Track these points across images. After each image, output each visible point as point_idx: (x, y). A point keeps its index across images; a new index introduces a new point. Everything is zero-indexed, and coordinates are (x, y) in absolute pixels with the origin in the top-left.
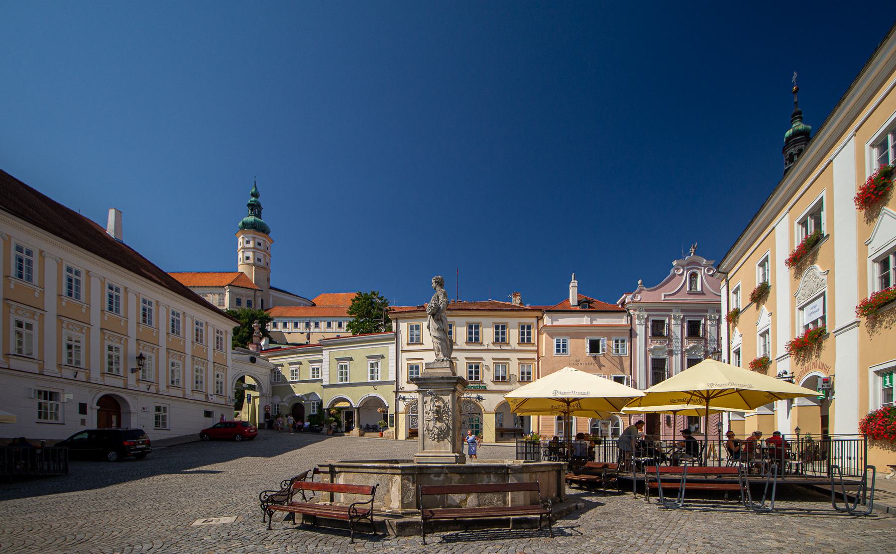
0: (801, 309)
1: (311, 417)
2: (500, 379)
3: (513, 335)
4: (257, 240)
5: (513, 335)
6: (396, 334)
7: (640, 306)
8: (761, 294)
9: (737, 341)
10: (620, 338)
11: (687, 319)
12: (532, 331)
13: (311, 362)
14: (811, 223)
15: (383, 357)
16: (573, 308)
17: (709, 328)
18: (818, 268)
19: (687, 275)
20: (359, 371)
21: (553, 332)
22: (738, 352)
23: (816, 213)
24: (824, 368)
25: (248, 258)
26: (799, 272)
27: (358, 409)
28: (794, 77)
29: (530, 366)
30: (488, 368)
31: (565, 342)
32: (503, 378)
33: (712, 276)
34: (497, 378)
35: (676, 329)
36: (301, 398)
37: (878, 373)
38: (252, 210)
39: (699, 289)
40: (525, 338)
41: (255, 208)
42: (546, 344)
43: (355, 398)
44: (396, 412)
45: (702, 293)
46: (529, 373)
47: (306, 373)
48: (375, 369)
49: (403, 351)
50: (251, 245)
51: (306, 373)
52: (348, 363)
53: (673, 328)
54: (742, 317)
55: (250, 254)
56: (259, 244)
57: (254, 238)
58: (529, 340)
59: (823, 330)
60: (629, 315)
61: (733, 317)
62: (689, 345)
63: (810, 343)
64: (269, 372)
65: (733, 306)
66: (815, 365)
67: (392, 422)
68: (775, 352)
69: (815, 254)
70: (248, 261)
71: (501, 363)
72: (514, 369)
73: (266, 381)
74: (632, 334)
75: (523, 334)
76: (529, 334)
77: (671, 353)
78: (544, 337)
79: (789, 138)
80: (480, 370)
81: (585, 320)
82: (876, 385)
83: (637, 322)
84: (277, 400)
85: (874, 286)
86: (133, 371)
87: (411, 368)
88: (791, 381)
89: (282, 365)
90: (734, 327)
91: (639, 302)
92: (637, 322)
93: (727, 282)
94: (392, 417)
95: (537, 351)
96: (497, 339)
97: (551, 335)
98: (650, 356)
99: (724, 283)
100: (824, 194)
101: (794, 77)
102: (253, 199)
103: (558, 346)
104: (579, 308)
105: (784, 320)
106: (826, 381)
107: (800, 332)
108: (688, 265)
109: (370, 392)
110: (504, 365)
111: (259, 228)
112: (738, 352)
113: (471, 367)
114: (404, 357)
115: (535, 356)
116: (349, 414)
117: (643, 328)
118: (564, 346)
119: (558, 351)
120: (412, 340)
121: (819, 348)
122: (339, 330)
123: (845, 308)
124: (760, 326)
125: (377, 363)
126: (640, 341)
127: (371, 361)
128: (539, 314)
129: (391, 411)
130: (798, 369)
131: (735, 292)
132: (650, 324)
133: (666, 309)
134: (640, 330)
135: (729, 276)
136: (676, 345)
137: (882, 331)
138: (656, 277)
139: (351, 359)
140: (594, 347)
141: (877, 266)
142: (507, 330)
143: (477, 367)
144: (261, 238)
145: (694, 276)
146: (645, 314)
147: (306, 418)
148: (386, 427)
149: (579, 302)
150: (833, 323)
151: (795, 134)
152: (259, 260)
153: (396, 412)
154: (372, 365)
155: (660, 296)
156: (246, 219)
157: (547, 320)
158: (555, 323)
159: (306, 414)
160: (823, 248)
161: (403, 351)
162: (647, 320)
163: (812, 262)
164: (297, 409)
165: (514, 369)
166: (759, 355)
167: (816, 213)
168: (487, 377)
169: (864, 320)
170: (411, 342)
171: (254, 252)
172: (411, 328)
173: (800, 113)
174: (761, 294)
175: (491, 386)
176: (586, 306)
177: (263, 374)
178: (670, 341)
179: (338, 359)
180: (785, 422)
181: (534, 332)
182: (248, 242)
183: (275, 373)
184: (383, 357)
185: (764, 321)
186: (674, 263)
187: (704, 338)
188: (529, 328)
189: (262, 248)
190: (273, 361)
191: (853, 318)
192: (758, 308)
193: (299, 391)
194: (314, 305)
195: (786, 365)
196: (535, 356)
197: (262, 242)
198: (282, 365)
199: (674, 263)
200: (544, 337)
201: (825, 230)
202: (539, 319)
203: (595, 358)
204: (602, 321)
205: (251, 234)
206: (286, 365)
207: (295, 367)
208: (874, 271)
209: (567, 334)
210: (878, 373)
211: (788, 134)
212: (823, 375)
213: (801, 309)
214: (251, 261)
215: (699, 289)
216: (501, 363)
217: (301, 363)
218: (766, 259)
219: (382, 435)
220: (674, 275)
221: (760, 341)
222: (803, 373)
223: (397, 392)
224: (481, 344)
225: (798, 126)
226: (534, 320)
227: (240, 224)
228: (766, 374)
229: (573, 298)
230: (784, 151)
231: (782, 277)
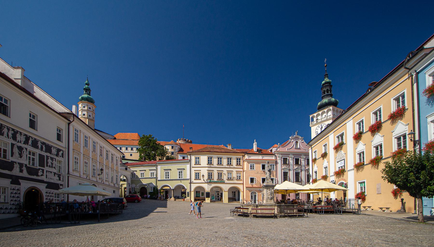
0: (338, 162)
1: (150, 193)
2: (229, 179)
3: (234, 162)
4: (89, 106)
5: (234, 162)
6: (190, 161)
7: (279, 153)
8: (324, 155)
9: (315, 169)
10: (272, 164)
11: (295, 158)
12: (241, 161)
13: (150, 170)
14: (340, 138)
15: (184, 169)
16: (256, 153)
17: (302, 161)
18: (342, 152)
19: (294, 142)
20: (174, 174)
21: (249, 161)
22: (316, 172)
23: (342, 135)
24: (344, 180)
25: (84, 115)
26: (337, 151)
27: (173, 190)
28: (325, 60)
29: (240, 173)
30: (225, 174)
31: (253, 165)
32: (231, 178)
33: (303, 142)
34: (229, 178)
35: (291, 161)
36: (146, 185)
37: (359, 183)
38: (86, 91)
39: (299, 147)
40: (238, 164)
41: (88, 90)
42: (246, 165)
43: (172, 185)
44: (190, 191)
45: (299, 149)
46: (240, 177)
47: (148, 174)
48: (181, 174)
49: (193, 167)
50: (86, 108)
51: (148, 174)
52: (169, 171)
53: (290, 161)
54: (317, 161)
55: (85, 113)
56: (90, 108)
57: (87, 105)
58: (240, 164)
59: (344, 170)
60: (275, 156)
61: (314, 160)
62: (296, 167)
63: (340, 173)
64: (130, 174)
65: (314, 157)
66: (342, 179)
67: (188, 195)
68: (329, 174)
69: (342, 148)
70: (84, 116)
71: (230, 173)
72: (234, 175)
73: (129, 177)
74: (276, 163)
75: (237, 162)
76: (240, 162)
77: (289, 170)
78: (246, 163)
79: (323, 84)
80: (222, 175)
81: (260, 157)
82: (359, 186)
83: (278, 158)
84: (134, 186)
85: (358, 161)
86: (99, 175)
87: (196, 174)
88: (335, 183)
89: (136, 171)
90: (314, 164)
91: (278, 151)
92: (278, 158)
93: (312, 148)
94: (188, 193)
95: (243, 168)
96: (228, 163)
97: (249, 163)
98: (283, 171)
99: (310, 148)
100: (344, 131)
101: (325, 60)
102: (87, 86)
103: (251, 167)
104: (257, 153)
105: (332, 164)
106: (346, 184)
107: (337, 170)
108: (295, 138)
109: (179, 183)
110: (231, 173)
111: (89, 100)
112: (316, 172)
113: (219, 174)
114: (193, 169)
115: (242, 170)
116: (167, 192)
117: (280, 161)
118: (253, 167)
119: (251, 168)
120: (196, 163)
121: (343, 174)
122: (131, 151)
123: (350, 165)
124: (324, 165)
125: (182, 172)
126: (279, 165)
127: (179, 171)
128: (243, 154)
129: (188, 190)
130: (337, 180)
131: (315, 152)
132: (282, 159)
133: (288, 154)
134: (279, 161)
135: (312, 146)
136: (291, 167)
137: (360, 172)
138: (283, 141)
139: (170, 170)
140: (263, 167)
141: (358, 155)
142: (232, 160)
143: (221, 174)
144: (91, 105)
145: (297, 142)
146: (281, 156)
147: (148, 194)
148: (185, 197)
149: (257, 150)
150: (347, 168)
151: (326, 83)
152: (90, 116)
153: (190, 191)
154: (179, 172)
155: (286, 149)
156: (83, 96)
157: (246, 157)
158: (250, 158)
159: (148, 192)
160: (344, 146)
161: (193, 167)
162: (281, 158)
163: (341, 150)
164: (143, 190)
165: (234, 175)
166: (324, 174)
167: (342, 135)
168: (225, 178)
169: (355, 169)
170: (196, 164)
171: (87, 112)
172: (196, 158)
173: (327, 75)
174: (324, 155)
175: (226, 181)
176: (260, 152)
177: (128, 174)
178: (289, 166)
179: (165, 170)
180: (333, 196)
181: (241, 161)
182: (84, 107)
183: (133, 175)
184: (184, 169)
185: (325, 164)
186: (290, 137)
187: (300, 165)
188: (240, 159)
189: (91, 110)
190: (132, 169)
191: (353, 168)
192: (323, 159)
193: (145, 182)
194: (115, 138)
195: (333, 178)
196: (242, 170)
197: (91, 107)
198: (136, 171)
199: (290, 137)
200: (246, 163)
201: (344, 141)
202: (243, 156)
203: (264, 171)
204: (266, 158)
205: (86, 103)
206: (138, 171)
207: (142, 172)
208: (357, 156)
209: (254, 162)
210: (359, 183)
211: (323, 82)
212: (345, 183)
213: (338, 162)
214: (86, 116)
215: (299, 147)
216: (230, 173)
217: (145, 171)
218: (326, 145)
219: (184, 200)
220: (290, 142)
221: (324, 170)
222: (338, 181)
223: (190, 183)
224: (223, 165)
225: (327, 80)
226: (241, 157)
227: (80, 98)
228: (326, 180)
229: (255, 148)
230: (322, 89)
231: (331, 152)
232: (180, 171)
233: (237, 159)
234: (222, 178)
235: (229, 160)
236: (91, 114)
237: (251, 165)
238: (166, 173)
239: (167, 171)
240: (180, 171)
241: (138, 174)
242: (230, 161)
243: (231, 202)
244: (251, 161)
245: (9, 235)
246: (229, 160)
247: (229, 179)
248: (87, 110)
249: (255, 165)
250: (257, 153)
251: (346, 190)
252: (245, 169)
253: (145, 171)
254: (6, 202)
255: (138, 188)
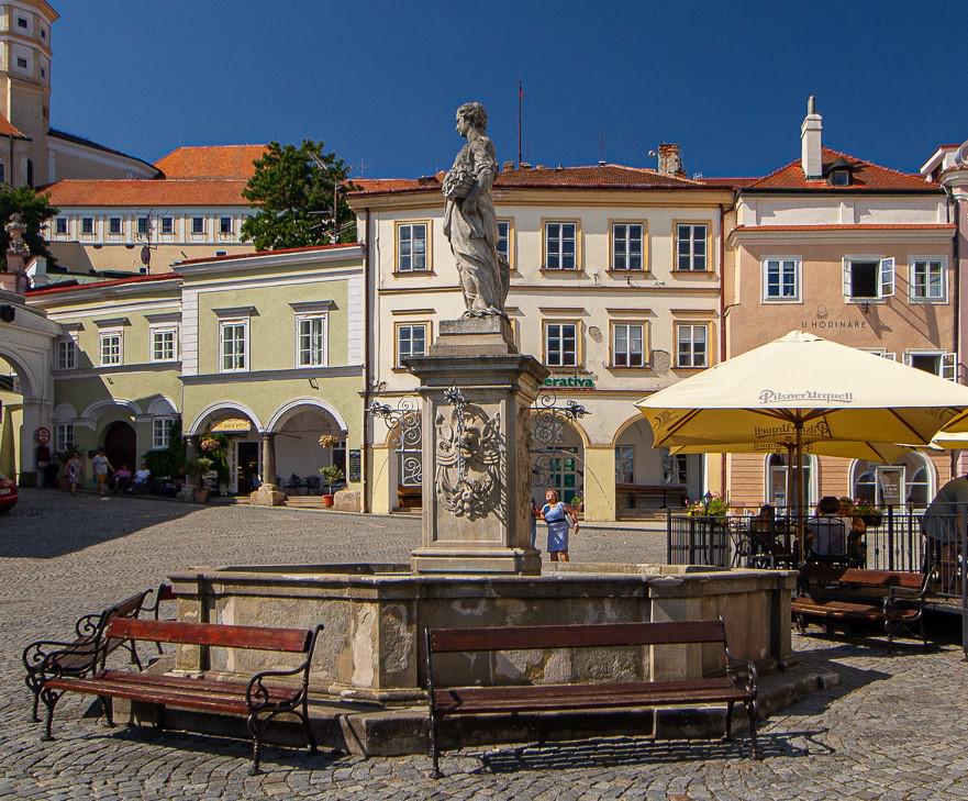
1: (153, 459)
2: (626, 362)
3: (661, 251)
4: (17, 14)
5: (661, 251)
6: (367, 249)
10: (928, 259)
12: (708, 241)
15: (332, 306)
16: (810, 184)
20: (274, 342)
21: (759, 242)
27: (271, 436)
31: (789, 268)
32: (636, 359)
34: (621, 358)
36: (128, 409)
40: (690, 260)
42: (743, 272)
43: (263, 409)
44: (367, 446)
46: (700, 347)
48: (313, 336)
49: (384, 292)
52: (245, 321)
56: (23, 23)
58: (700, 263)
64: (45, 343)
67: (355, 469)
72: (662, 337)
73: (39, 365)
75: (684, 248)
76: (700, 248)
78: (738, 255)
80: (577, 338)
81: (840, 214)
84: (68, 413)
87: (405, 333)
89: (80, 327)
94: (355, 457)
95: (721, 291)
96: (620, 262)
97: (756, 252)
103: (773, 278)
104: (825, 184)
110: (636, 327)
113: (554, 332)
114: (385, 305)
115: (714, 303)
116: (249, 448)
119: (773, 291)
120: (405, 263)
122: (222, 239)
127: (302, 317)
128: (726, 198)
129: (354, 442)
139: (253, 312)
140: (864, 280)
142: (644, 240)
143: (569, 332)
147: (139, 460)
152: (22, 63)
154: (306, 326)
157: (745, 214)
158: (766, 222)
159: (141, 450)
164: (119, 435)
172: (405, 233)
175: (606, 380)
176: (842, 179)
179: (220, 313)
181: (712, 243)
183: (62, 345)
184: (332, 306)
188: (700, 233)
189: (29, 31)
190: (57, 316)
193: (124, 390)
194: (161, 175)
198: (80, 327)
200: (738, 255)
202: (726, 210)
203: (866, 309)
206: (89, 326)
207: (112, 332)
216: (629, 323)
217: (126, 322)
219: (330, 503)
223: (368, 394)
224: (581, 273)
232: (311, 316)
233: (684, 232)
234: (578, 361)
235: (627, 242)
236: (28, 54)
237: (773, 268)
238: (229, 331)
239: (234, 323)
240: (311, 316)
241: (90, 344)
242: (636, 247)
243: (631, 518)
244: (778, 239)
245: (53, 608)
246: (627, 242)
247: (626, 362)
248: (10, 32)
249: (801, 268)
250: (825, 184)
251: (955, 505)
252: (736, 293)
253: (126, 322)
254: (823, 469)
255: (91, 426)
